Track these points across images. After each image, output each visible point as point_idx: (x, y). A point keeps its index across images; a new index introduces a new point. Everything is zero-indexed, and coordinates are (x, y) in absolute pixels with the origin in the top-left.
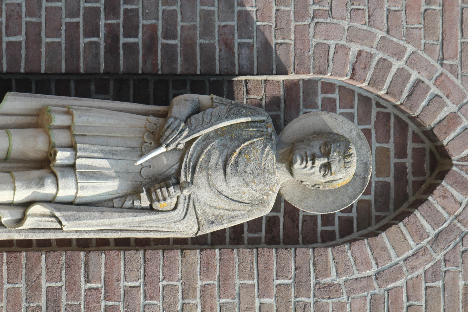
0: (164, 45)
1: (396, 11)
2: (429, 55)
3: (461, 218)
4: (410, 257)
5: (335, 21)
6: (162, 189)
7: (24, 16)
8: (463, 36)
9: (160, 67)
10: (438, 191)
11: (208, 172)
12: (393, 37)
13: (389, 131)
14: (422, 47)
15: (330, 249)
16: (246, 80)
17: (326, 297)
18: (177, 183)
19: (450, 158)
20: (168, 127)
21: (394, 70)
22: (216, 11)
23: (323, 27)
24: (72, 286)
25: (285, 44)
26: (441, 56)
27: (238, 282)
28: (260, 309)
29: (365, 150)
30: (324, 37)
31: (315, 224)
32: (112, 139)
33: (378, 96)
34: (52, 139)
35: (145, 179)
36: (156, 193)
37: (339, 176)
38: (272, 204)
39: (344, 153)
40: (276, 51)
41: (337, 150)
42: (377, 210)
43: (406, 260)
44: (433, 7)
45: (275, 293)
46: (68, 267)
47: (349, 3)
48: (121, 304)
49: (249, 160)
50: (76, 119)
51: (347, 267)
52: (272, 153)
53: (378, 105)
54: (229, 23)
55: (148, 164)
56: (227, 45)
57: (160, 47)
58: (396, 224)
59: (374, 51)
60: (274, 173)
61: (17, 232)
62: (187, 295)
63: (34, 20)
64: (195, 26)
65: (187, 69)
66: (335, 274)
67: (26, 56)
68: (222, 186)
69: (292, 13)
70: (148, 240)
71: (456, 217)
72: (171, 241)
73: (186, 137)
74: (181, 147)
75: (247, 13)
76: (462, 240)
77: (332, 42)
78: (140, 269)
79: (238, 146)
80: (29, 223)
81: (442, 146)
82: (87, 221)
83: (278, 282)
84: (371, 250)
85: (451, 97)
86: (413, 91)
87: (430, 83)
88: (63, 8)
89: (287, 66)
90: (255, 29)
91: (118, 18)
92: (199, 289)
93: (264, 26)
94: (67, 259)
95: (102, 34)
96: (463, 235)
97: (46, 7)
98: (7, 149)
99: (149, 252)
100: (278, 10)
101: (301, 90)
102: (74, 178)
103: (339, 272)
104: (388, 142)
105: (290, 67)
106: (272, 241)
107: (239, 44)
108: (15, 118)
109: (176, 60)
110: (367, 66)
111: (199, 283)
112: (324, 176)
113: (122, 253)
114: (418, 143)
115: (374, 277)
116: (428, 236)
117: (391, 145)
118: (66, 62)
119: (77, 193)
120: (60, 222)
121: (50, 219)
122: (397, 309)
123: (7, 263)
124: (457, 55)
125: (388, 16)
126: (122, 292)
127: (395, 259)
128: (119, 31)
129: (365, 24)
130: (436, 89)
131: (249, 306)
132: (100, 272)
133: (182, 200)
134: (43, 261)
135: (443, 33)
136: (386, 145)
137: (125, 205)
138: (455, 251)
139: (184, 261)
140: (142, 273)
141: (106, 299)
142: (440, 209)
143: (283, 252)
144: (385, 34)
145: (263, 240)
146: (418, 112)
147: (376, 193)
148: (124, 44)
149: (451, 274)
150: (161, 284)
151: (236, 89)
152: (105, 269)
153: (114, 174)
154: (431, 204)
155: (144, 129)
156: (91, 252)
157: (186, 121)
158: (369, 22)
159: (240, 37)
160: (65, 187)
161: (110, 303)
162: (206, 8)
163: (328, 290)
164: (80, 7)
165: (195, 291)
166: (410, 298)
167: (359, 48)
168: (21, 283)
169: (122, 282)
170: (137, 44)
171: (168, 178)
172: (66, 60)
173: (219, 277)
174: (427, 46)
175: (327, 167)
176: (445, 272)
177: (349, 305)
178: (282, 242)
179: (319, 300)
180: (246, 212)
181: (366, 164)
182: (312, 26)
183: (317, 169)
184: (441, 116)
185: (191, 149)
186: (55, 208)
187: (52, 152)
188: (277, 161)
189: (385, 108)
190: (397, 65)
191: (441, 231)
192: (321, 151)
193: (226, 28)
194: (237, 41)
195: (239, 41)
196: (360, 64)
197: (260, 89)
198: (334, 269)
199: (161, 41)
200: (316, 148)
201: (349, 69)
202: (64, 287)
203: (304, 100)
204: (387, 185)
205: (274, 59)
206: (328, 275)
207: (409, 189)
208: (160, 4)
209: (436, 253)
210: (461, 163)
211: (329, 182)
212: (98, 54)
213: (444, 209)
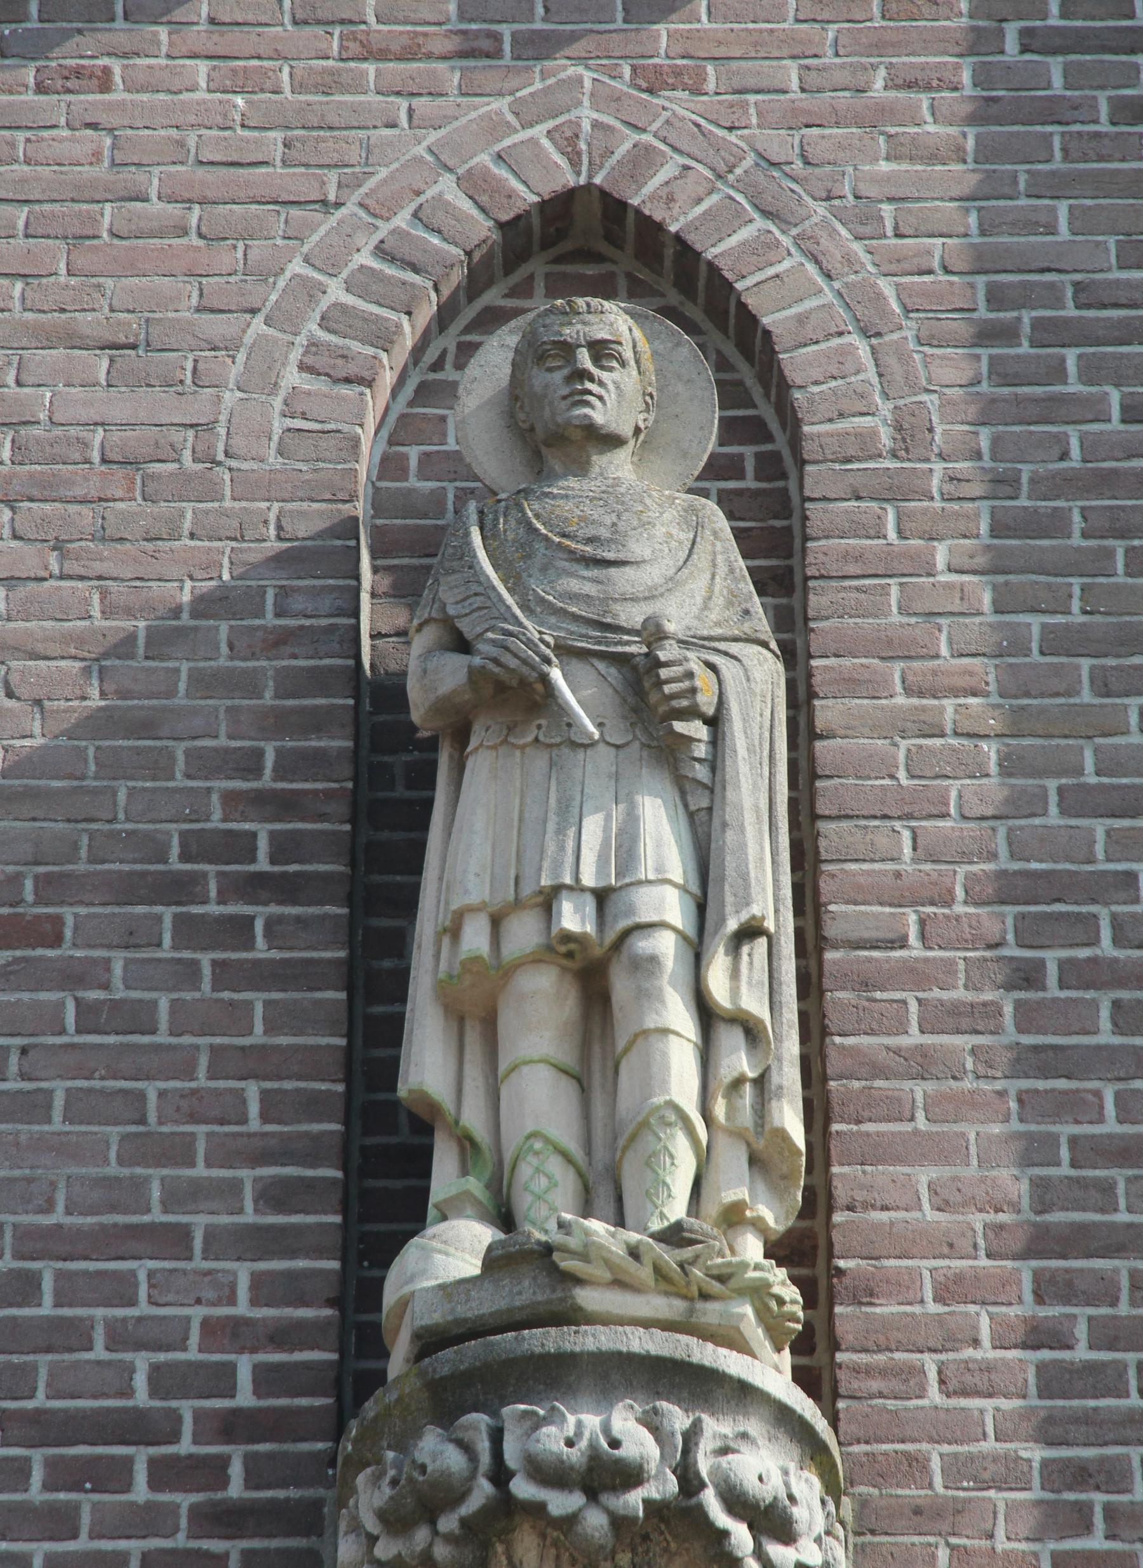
1: (201, 295)
4: (821, 268)
5: (223, 418)
6: (663, 677)
7: (193, 1085)
8: (267, 163)
11: (615, 600)
12: (266, 300)
15: (806, 429)
16: (372, 637)
17: (928, 436)
20: (496, 661)
21: (350, 300)
22: (192, 664)
23: (238, 443)
24: (917, 976)
26: (317, 206)
28: (962, 572)
30: (265, 440)
31: (739, 493)
32: (527, 815)
35: (635, 737)
39: (567, 313)
40: (297, 539)
41: (556, 328)
43: (828, 276)
44: (194, 222)
45: (921, 542)
46: (866, 985)
47: (180, 389)
48: (962, 870)
49: (582, 519)
50: (474, 899)
51: (851, 392)
53: (438, 366)
56: (279, 641)
58: (740, 295)
59: (301, 340)
61: (781, 1042)
62: (932, 725)
63: (203, 1061)
64: (229, 709)
65: (343, 726)
66: (869, 418)
67: (300, 1078)
72: (794, 795)
77: (276, 424)
78: (866, 827)
80: (755, 1004)
82: (750, 858)
83: (892, 535)
84: (805, 345)
85: (418, 184)
86: (403, 261)
88: (175, 996)
90: (240, 583)
92: (915, 701)
93: (231, 563)
94: (843, 989)
96: (763, 164)
97: (171, 1034)
98: (553, 1071)
100: (192, 536)
103: (865, 410)
105: (339, 511)
107: (278, 615)
109: (317, 750)
110: (340, 352)
112: (623, 364)
114: (532, 288)
115: (874, 341)
116: (769, 232)
118: (319, 989)
119: (675, 885)
121: (745, 958)
122: (953, 293)
123: (858, 1122)
124: (314, 174)
127: (829, 296)
128: (238, 872)
129: (233, 357)
130: (399, 216)
131: (958, 595)
132: (876, 916)
134: (850, 1041)
135: (259, 203)
137: (706, 781)
138: (806, 179)
139: (843, 732)
140: (876, 823)
141: (949, 902)
142: (699, 210)
144: (259, 319)
145: (784, 601)
150: (904, 782)
152: (869, 904)
153: (621, 807)
154: (687, 225)
155: (502, 750)
156: (826, 934)
158: (226, 349)
160: (660, 906)
161: (960, 893)
162: (182, 686)
163: (910, 434)
164: (173, 959)
166: (924, 267)
168: (912, 1091)
169: (904, 867)
173: (882, 658)
174: (290, 233)
176: (857, 197)
178: (787, 562)
179: (936, 450)
180: (718, 544)
182: (234, 464)
183: (605, 376)
184: (466, 205)
186: (716, 932)
187: (563, 949)
189: (444, 352)
190: (336, 292)
191: (756, 206)
192: (559, 368)
193: (236, 643)
194: (270, 619)
195: (270, 614)
198: (856, 419)
199: (267, 780)
201: (345, 391)
202: (920, 995)
203: (425, 516)
205: (319, 543)
206: (874, 433)
209: (810, 216)
212: (298, 919)
213: (699, 201)
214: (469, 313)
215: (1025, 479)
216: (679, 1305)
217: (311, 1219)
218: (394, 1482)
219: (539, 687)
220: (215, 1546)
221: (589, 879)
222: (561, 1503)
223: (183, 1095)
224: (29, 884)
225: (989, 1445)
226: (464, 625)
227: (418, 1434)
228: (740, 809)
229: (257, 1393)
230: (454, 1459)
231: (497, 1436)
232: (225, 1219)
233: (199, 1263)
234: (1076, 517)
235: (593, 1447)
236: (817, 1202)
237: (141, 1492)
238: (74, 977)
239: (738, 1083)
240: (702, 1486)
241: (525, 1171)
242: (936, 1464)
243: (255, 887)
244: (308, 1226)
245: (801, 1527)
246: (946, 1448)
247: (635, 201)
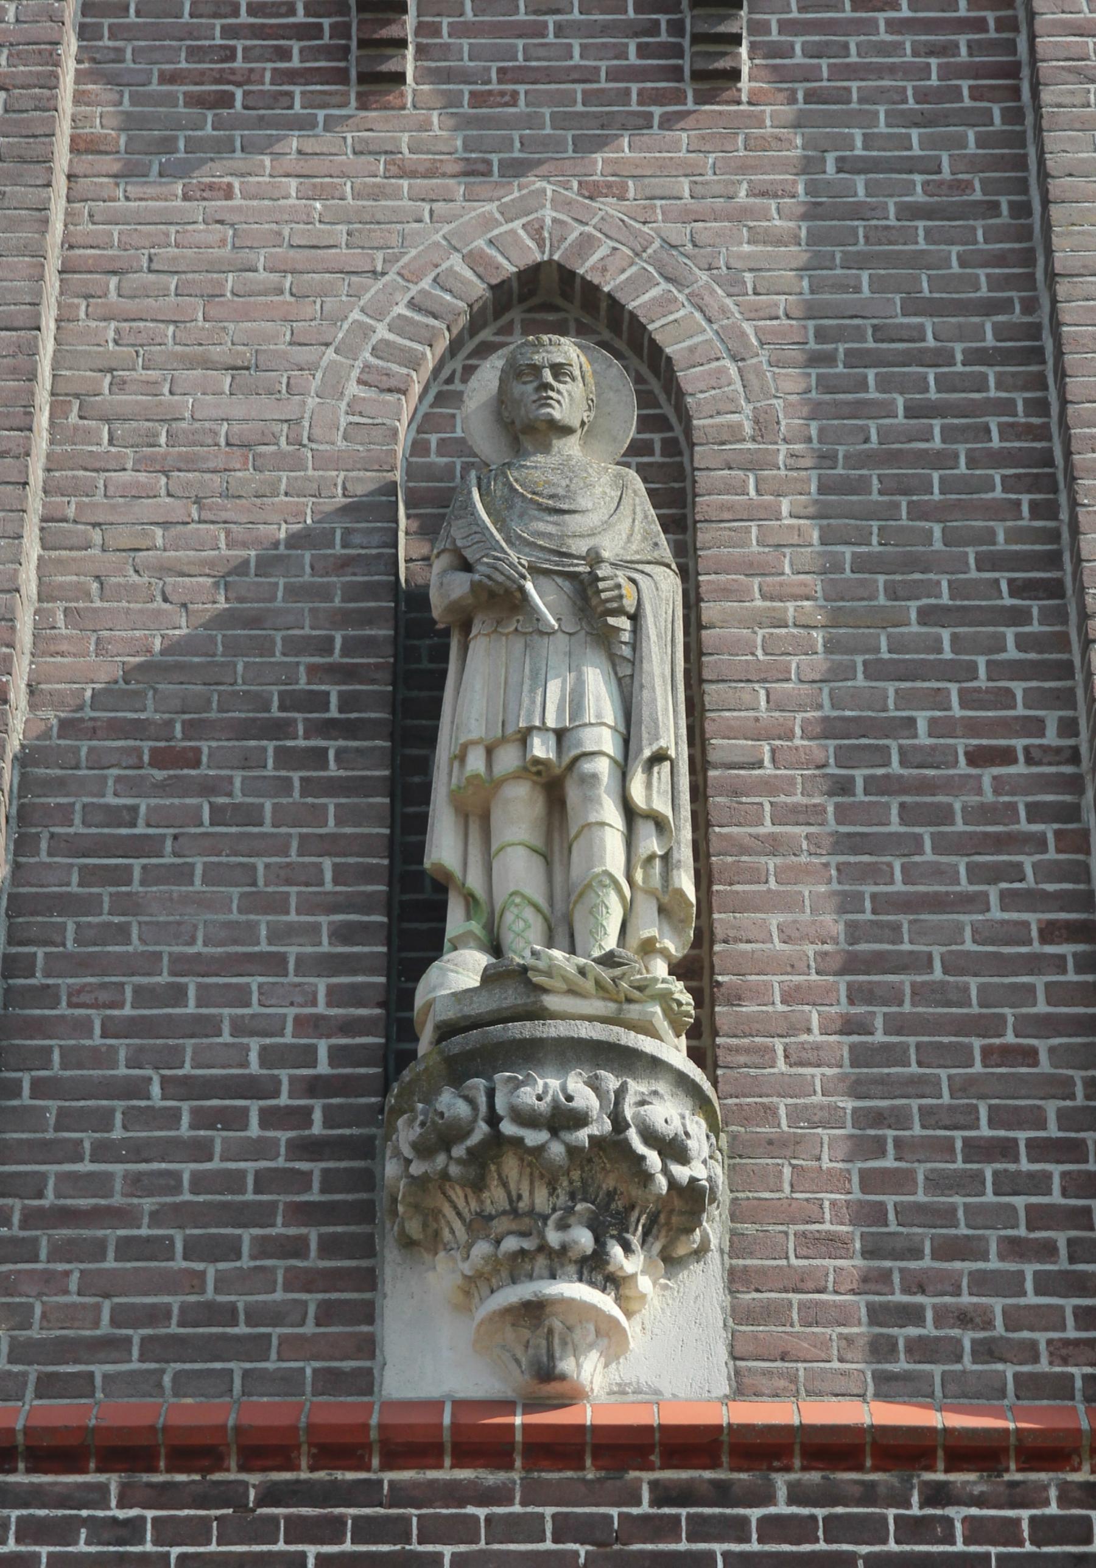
3: (639, 248)
21: (391, 337)
23: (317, 432)
24: (769, 787)
43: (710, 321)
46: (736, 793)
48: (799, 716)
50: (474, 736)
53: (450, 380)
56: (344, 564)
59: (359, 364)
63: (295, 844)
64: (311, 610)
70: (687, 673)
80: (662, 806)
91: (295, 720)
92: (768, 604)
95: (323, 743)
107: (344, 547)
108: (471, 848)
112: (573, 379)
126: (777, 714)
132: (742, 747)
142: (623, 277)
143: (701, 487)
144: (331, 349)
148: (340, 711)
161: (798, 731)
162: (280, 594)
163: (764, 426)
183: (561, 387)
184: (469, 274)
190: (382, 332)
194: (338, 550)
199: (336, 657)
201: (389, 397)
203: (441, 480)
206: (740, 425)
212: (357, 750)
213: (623, 271)
214: (470, 346)
215: (840, 456)
216: (613, 1006)
217: (366, 949)
218: (423, 1124)
219: (518, 595)
220: (303, 1166)
221: (551, 723)
222: (534, 1138)
223: (281, 866)
224: (178, 727)
225: (818, 1099)
226: (468, 554)
227: (438, 1092)
228: (652, 675)
229: (331, 1064)
230: (462, 1109)
231: (491, 1094)
232: (309, 949)
233: (292, 978)
234: (875, 481)
235: (555, 1100)
236: (704, 937)
237: (254, 1130)
238: (208, 788)
239: (651, 858)
240: (628, 1126)
241: (509, 917)
242: (782, 1111)
243: (329, 728)
244: (365, 954)
245: (693, 1153)
246: (789, 1101)
247: (581, 271)
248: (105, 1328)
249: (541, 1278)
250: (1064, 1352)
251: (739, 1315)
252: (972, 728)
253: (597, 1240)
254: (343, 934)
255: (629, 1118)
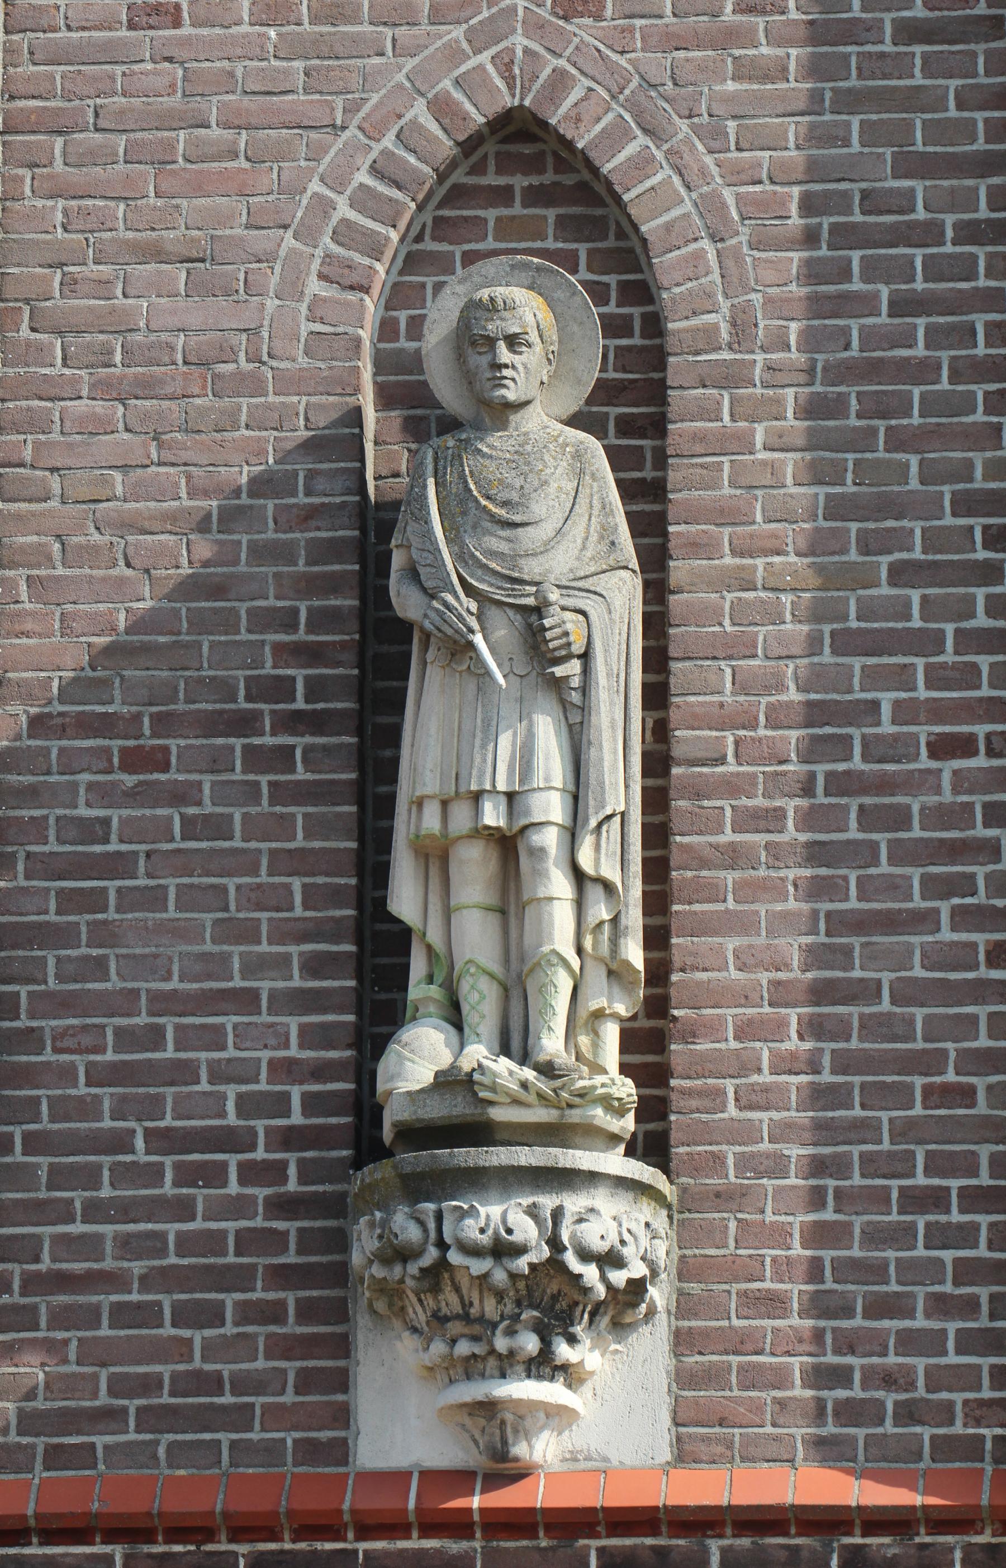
0: (308, 632)
2: (326, 152)
3: (615, 89)
5: (266, 323)
7: (258, 880)
9: (346, 637)
10: (568, 132)
13: (466, 219)
14: (312, 164)
18: (538, 610)
19: (511, 110)
21: (353, 215)
24: (732, 787)
25: (306, 413)
27: (727, 491)
29: (489, 267)
31: (629, 349)
33: (402, 240)
34: (465, 832)
36: (555, 649)
37: (530, 319)
38: (582, 435)
42: (606, 237)
43: (689, 188)
44: (243, 146)
46: (699, 796)
48: (764, 700)
50: (428, 790)
52: (490, 440)
53: (419, 238)
54: (270, 513)
55: (507, 664)
56: (309, 515)
57: (312, 638)
59: (319, 252)
60: (526, 434)
63: (264, 862)
64: (275, 575)
67: (327, 875)
68: (546, 530)
69: (253, 400)
71: (613, 97)
73: (457, 598)
74: (473, 606)
75: (253, 481)
76: (654, 86)
79: (477, 501)
80: (611, 872)
81: (488, 123)
83: (726, 417)
87: (377, 148)
88: (245, 810)
89: (346, 409)
91: (261, 712)
92: (738, 561)
94: (683, 798)
99: (673, 652)
100: (247, 427)
101: (392, 378)
102: (530, 795)
104: (486, 220)
106: (657, 426)
108: (430, 895)
111: (728, 560)
112: (529, 346)
113: (674, 699)
115: (719, 245)
117: (491, 215)
120: (609, 818)
121: (604, 834)
123: (690, 903)
125: (257, 228)
126: (741, 698)
127: (688, 207)
132: (706, 739)
133: (570, 602)
136: (491, 224)
138: (674, 99)
140: (709, 663)
141: (754, 727)
142: (598, 128)
144: (290, 233)
145: (658, 443)
146: (427, 169)
147: (576, 241)
148: (307, 702)
149: (714, 105)
151: (390, 496)
154: (590, 142)
157: (432, 595)
159: (294, 494)
160: (546, 811)
161: (762, 719)
162: (243, 556)
163: (742, 327)
165: (742, 568)
167: (313, 278)
170: (307, 678)
171: (529, 626)
172: (334, 804)
174: (310, 156)
175: (513, 341)
177: (769, 290)
181: (512, 267)
182: (274, 363)
183: (517, 359)
184: (434, 127)
185: (481, 586)
188: (505, 429)
189: (424, 226)
190: (344, 210)
191: (638, 124)
194: (302, 499)
195: (301, 495)
196: (342, 276)
197: (391, 451)
199: (301, 635)
200: (480, 361)
201: (351, 297)
203: (411, 373)
204: (560, 220)
206: (716, 327)
207: (569, 180)
208: (238, 638)
210: (518, 91)
211: (541, 336)
212: (325, 748)
213: (598, 120)
230: (413, 1233)
237: (233, 1188)
242: (730, 1161)
248: (103, 1399)
249: (492, 1377)
250: (978, 1413)
251: (684, 1379)
252: (937, 712)
253: (543, 1339)
254: (314, 966)
255: (566, 1243)
